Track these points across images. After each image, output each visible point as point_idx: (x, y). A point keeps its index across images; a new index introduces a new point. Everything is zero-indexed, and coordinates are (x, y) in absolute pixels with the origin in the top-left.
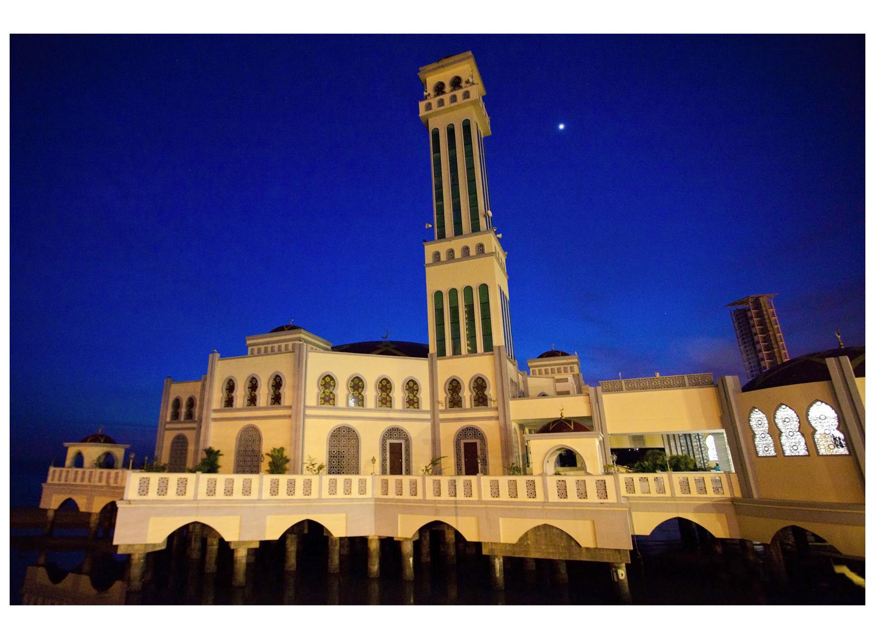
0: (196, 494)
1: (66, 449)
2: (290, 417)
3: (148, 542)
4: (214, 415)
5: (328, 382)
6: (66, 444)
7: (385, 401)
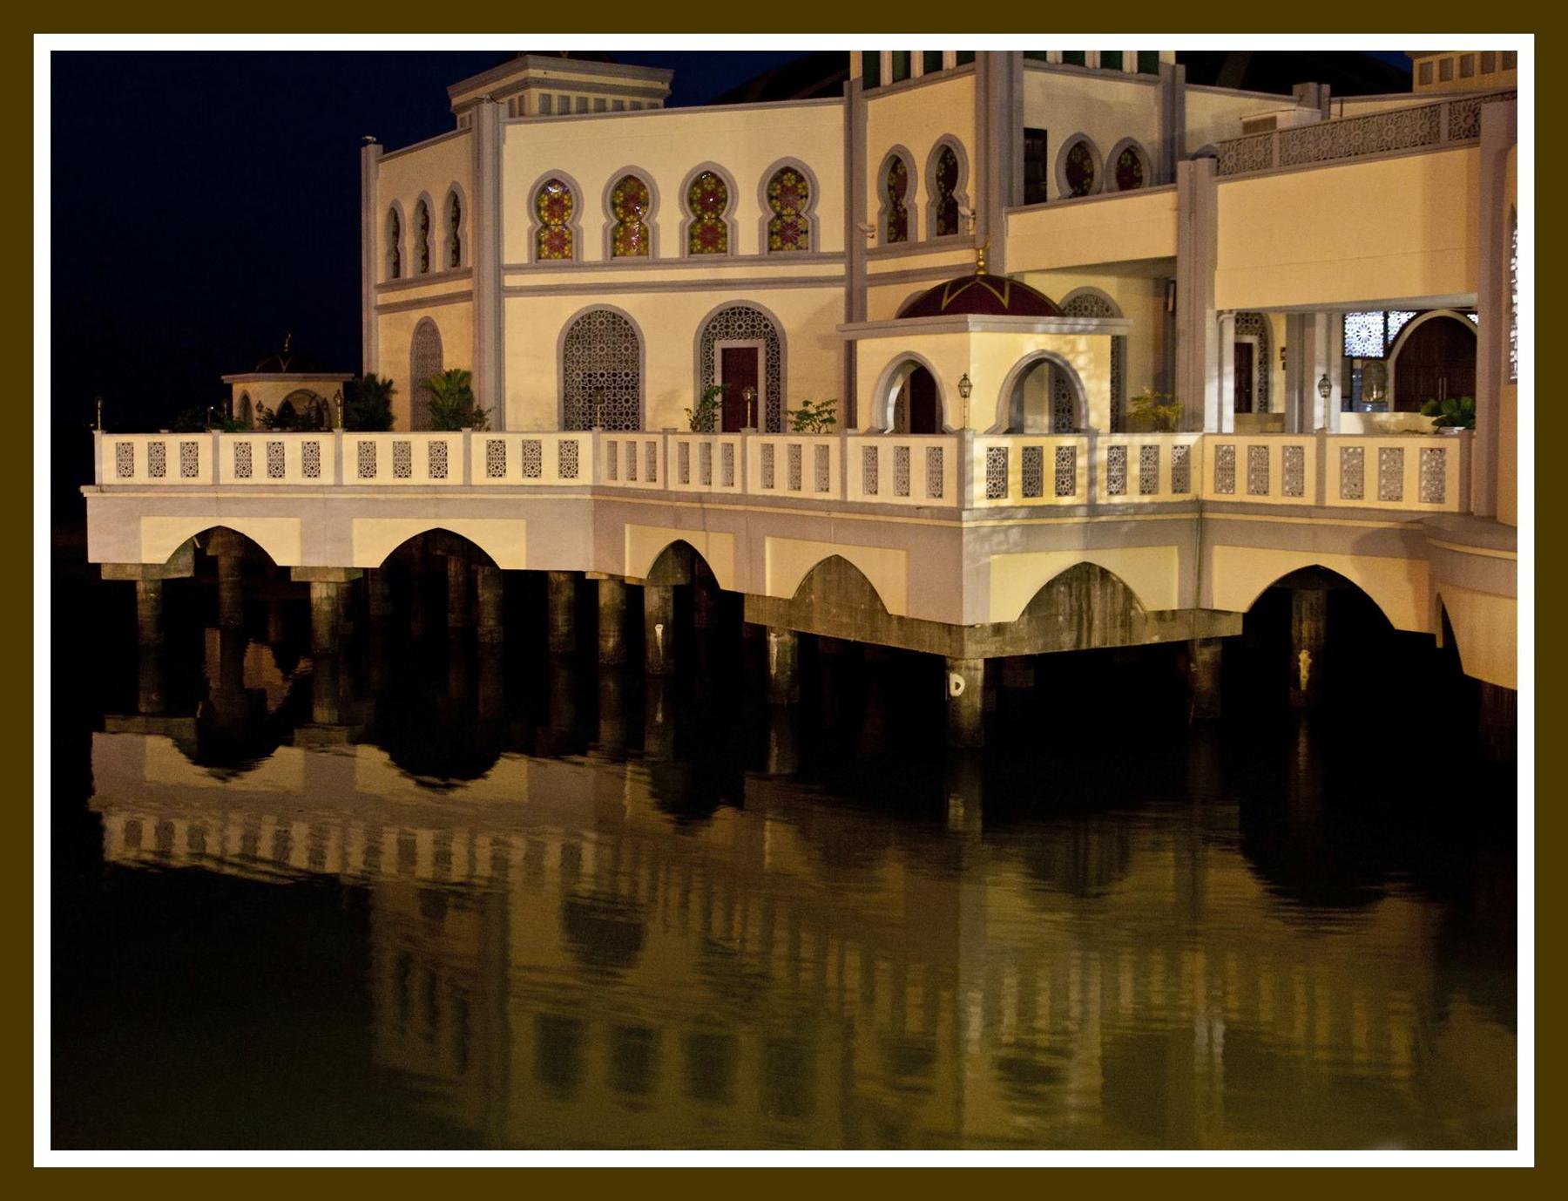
0: (216, 475)
1: (230, 387)
2: (466, 296)
3: (356, 565)
4: (381, 299)
5: (554, 201)
6: (226, 379)
7: (708, 236)
